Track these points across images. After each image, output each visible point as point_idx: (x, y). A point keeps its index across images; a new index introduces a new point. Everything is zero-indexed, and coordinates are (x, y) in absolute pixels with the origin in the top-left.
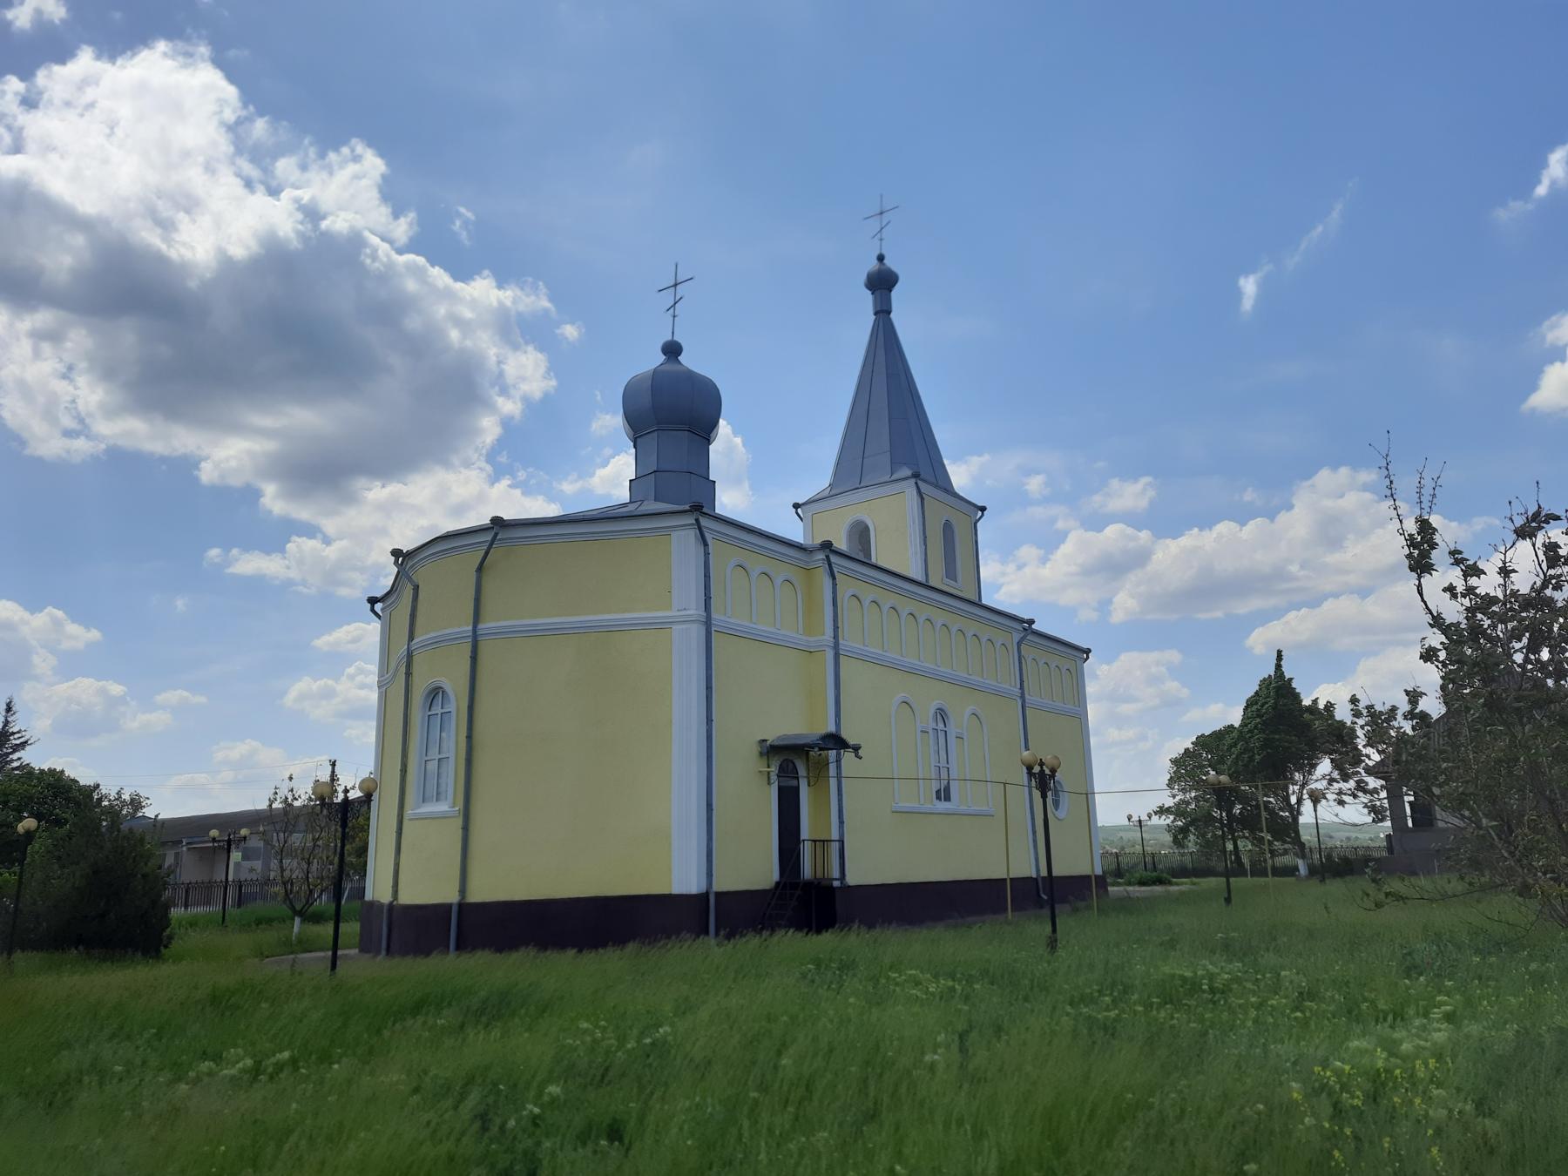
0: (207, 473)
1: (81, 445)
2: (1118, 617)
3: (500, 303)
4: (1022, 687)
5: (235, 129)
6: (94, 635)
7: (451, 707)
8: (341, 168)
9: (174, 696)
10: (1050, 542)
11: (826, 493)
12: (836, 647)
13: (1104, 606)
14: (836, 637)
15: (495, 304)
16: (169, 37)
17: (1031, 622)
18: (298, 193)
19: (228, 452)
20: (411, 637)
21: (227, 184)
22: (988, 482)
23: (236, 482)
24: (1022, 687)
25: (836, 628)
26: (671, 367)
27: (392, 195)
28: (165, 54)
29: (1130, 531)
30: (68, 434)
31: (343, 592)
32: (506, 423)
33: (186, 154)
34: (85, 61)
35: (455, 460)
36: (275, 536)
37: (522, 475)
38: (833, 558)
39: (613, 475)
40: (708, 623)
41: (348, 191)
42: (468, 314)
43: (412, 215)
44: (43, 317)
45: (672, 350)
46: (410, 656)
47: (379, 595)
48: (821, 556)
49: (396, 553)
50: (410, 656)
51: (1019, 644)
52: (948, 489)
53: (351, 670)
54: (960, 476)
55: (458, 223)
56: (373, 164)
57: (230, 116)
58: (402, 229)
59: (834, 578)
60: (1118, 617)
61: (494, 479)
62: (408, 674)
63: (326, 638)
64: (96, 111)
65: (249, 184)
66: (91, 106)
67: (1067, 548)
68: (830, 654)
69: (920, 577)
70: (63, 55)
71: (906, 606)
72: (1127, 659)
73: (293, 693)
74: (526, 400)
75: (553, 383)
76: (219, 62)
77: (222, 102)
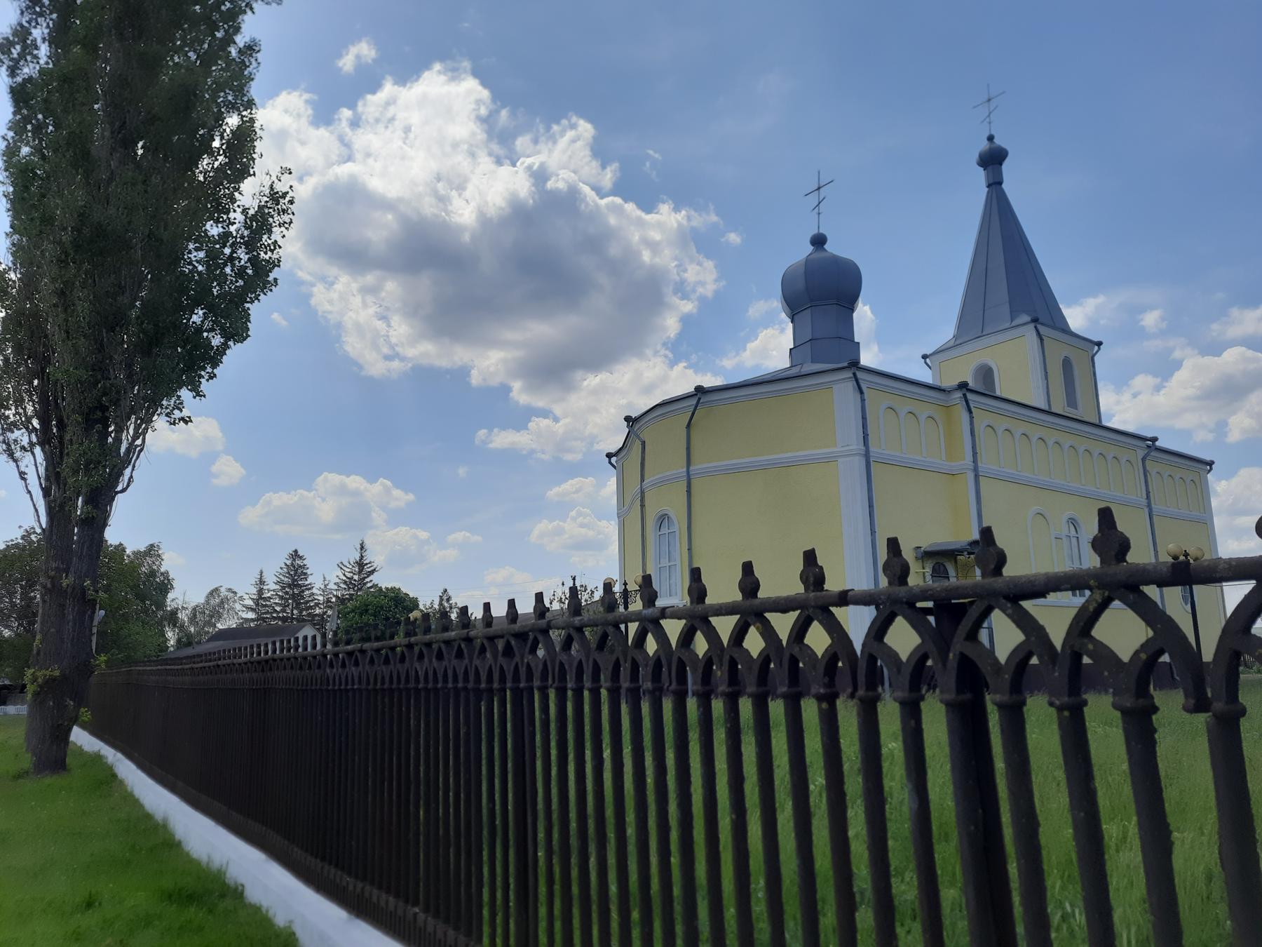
0: (475, 379)
1: (396, 364)
2: (1234, 436)
3: (680, 225)
4: (1148, 497)
5: (487, 122)
6: (411, 497)
7: (675, 528)
8: (562, 136)
9: (459, 536)
10: (1165, 369)
11: (952, 343)
12: (976, 470)
13: (1221, 427)
14: (975, 461)
15: (675, 225)
16: (442, 59)
17: (1154, 439)
18: (529, 161)
19: (489, 362)
20: (642, 480)
21: (486, 162)
22: (1102, 322)
23: (495, 382)
24: (1148, 497)
25: (975, 454)
26: (820, 255)
27: (600, 152)
28: (439, 72)
29: (1250, 353)
30: (388, 358)
31: (568, 457)
32: (686, 320)
33: (455, 145)
34: (389, 88)
35: (649, 352)
36: (520, 418)
37: (694, 357)
38: (970, 396)
39: (772, 345)
40: (867, 455)
41: (566, 154)
42: (656, 236)
43: (615, 165)
44: (370, 278)
45: (819, 241)
46: (642, 493)
47: (613, 449)
48: (958, 395)
49: (627, 419)
50: (642, 493)
51: (1144, 460)
52: (1065, 330)
53: (573, 513)
54: (1076, 317)
55: (648, 164)
56: (585, 129)
57: (483, 111)
58: (608, 177)
59: (970, 412)
60: (1234, 436)
61: (672, 364)
62: (642, 506)
63: (556, 490)
64: (397, 123)
65: (499, 162)
66: (393, 119)
67: (1181, 375)
68: (971, 476)
69: (1043, 406)
70: (375, 87)
71: (1035, 432)
72: (1245, 474)
73: (536, 532)
74: (703, 300)
75: (723, 283)
76: (476, 73)
77: (479, 102)
